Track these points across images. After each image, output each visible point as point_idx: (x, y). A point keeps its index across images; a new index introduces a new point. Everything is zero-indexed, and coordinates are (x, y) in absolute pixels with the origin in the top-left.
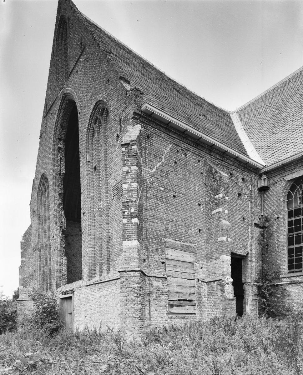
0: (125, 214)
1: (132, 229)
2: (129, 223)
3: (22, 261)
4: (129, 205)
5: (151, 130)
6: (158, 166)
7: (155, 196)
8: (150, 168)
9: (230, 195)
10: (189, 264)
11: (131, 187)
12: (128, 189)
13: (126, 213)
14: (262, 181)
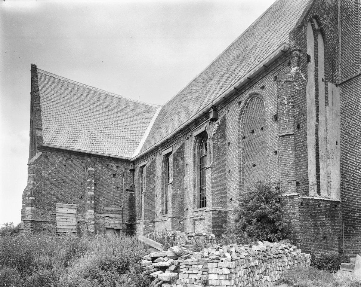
2: (29, 199)
3: (23, 206)
5: (48, 153)
10: (73, 214)
13: (27, 195)
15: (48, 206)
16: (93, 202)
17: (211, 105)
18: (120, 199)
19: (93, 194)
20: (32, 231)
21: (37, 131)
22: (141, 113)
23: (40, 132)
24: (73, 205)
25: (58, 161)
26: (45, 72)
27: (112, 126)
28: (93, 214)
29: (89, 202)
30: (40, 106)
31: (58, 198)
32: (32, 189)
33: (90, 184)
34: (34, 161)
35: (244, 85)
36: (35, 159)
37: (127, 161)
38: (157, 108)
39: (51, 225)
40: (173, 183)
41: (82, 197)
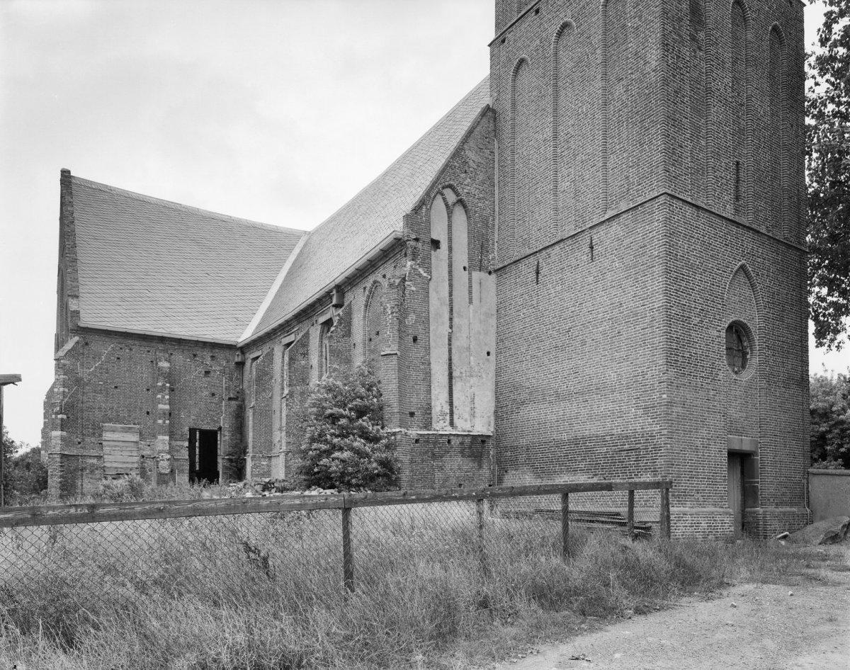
2: (56, 417)
3: (45, 423)
15: (88, 428)
16: (167, 422)
17: (333, 285)
19: (167, 407)
20: (63, 471)
21: (70, 299)
23: (75, 301)
24: (132, 426)
28: (167, 442)
30: (75, 253)
32: (62, 400)
33: (162, 389)
34: (66, 354)
35: (366, 267)
37: (230, 347)
38: (299, 237)
39: (95, 461)
40: (288, 397)
41: (148, 413)
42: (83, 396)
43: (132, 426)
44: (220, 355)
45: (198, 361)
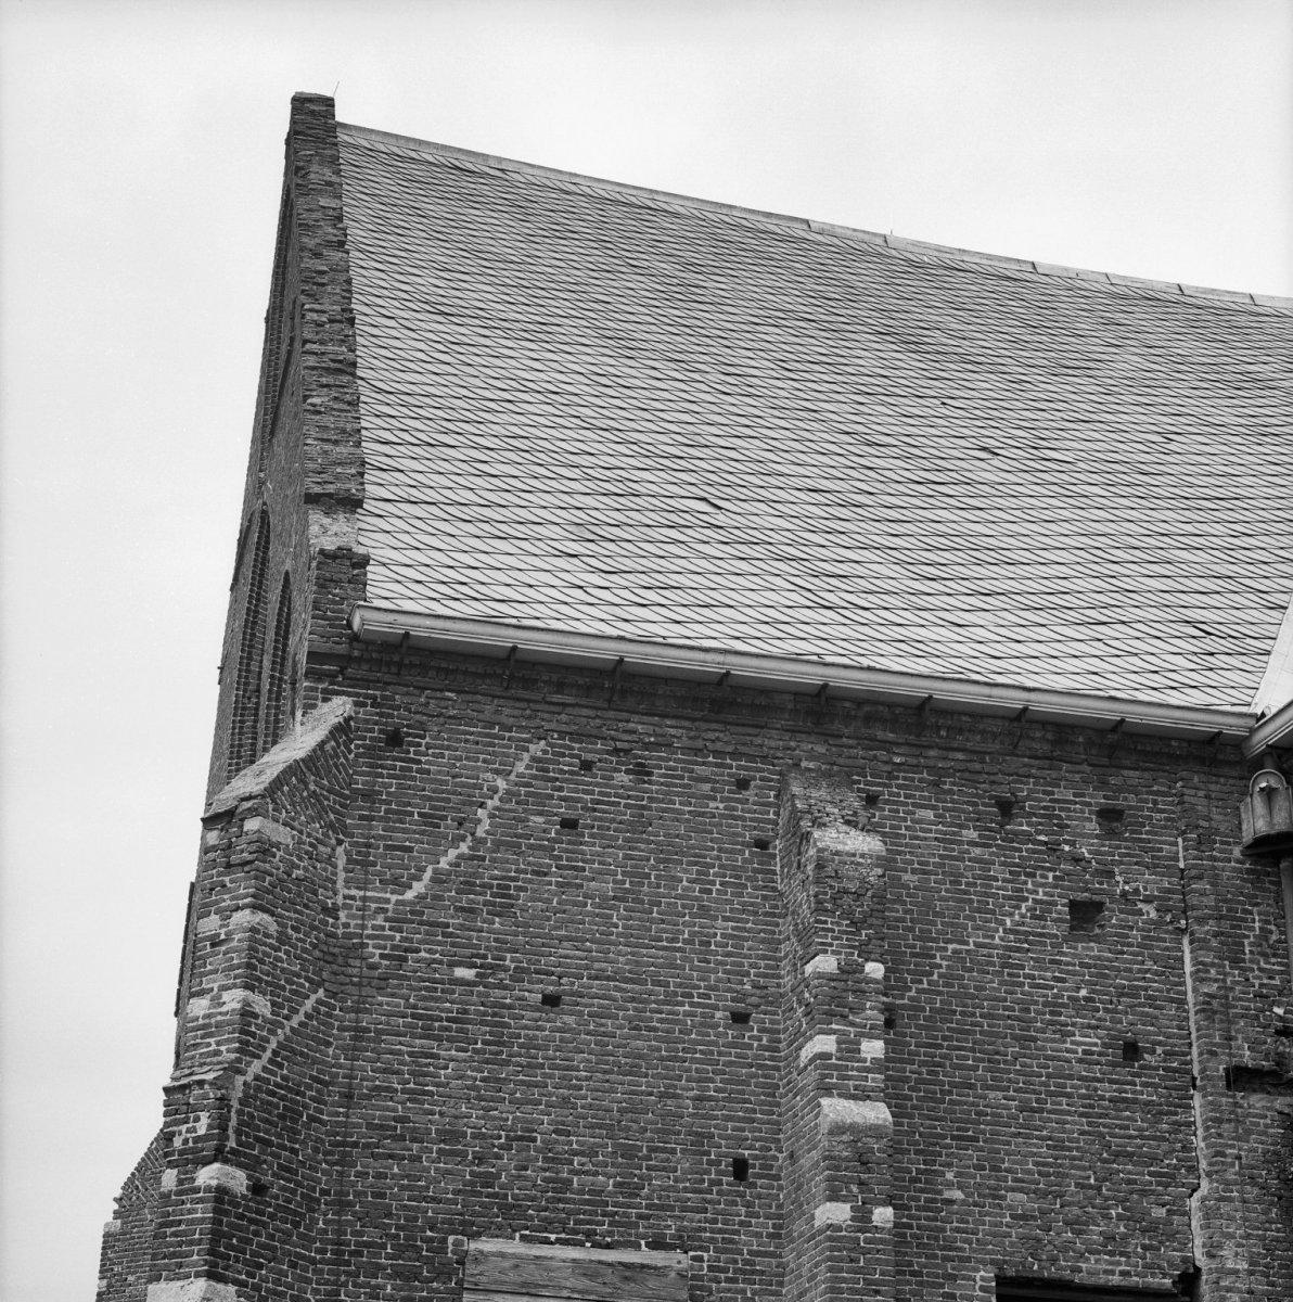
0: (175, 1145)
1: (192, 1222)
2: (186, 1187)
4: (191, 1101)
6: (444, 864)
7: (413, 1016)
8: (395, 881)
9: (1002, 923)
11: (219, 1010)
12: (207, 1021)
14: (1259, 804)
18: (1168, 1179)
22: (1241, 368)
24: (644, 1256)
25: (501, 784)
26: (393, 141)
27: (987, 472)
29: (837, 1213)
31: (488, 1180)
32: (234, 1069)
36: (281, 767)
41: (740, 1169)
42: (353, 1052)
43: (644, 1256)
44: (1153, 801)
45: (1028, 837)
